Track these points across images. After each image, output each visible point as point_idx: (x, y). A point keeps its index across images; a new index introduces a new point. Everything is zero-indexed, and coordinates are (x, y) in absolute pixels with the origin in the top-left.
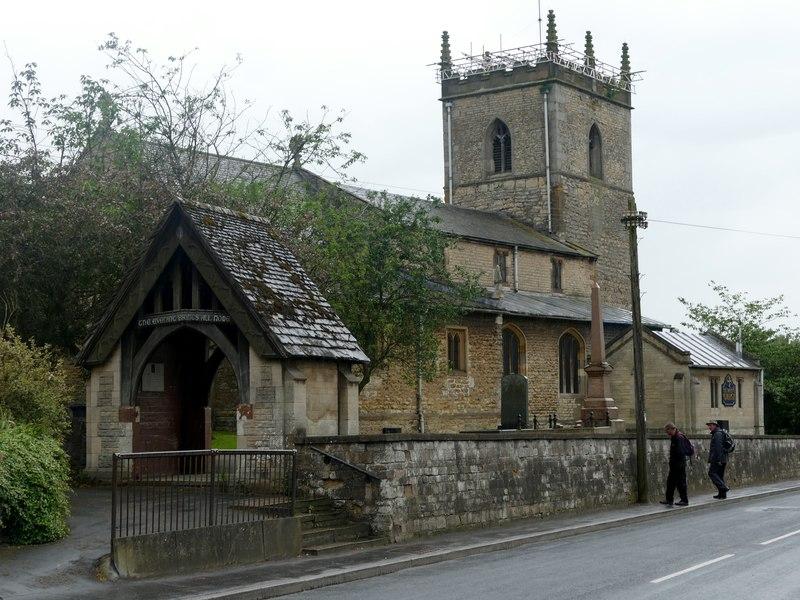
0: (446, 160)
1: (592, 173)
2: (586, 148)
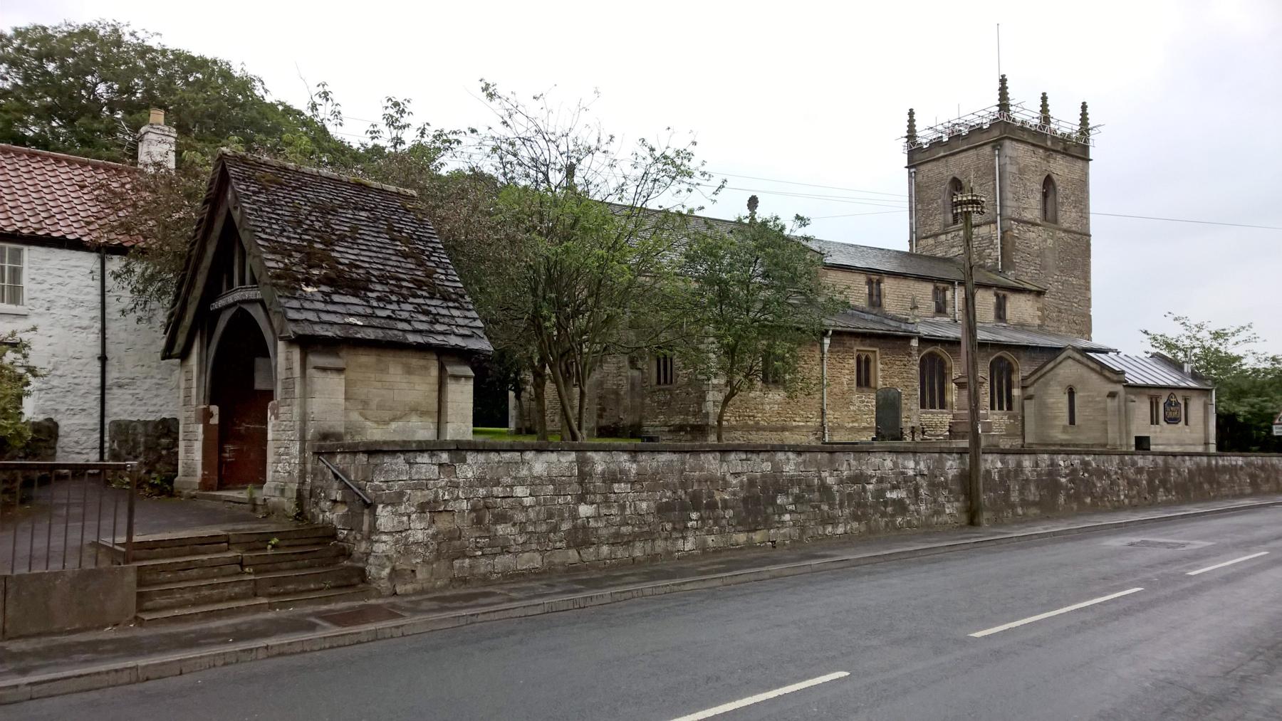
0: (911, 218)
1: (1045, 218)
2: (1039, 196)
